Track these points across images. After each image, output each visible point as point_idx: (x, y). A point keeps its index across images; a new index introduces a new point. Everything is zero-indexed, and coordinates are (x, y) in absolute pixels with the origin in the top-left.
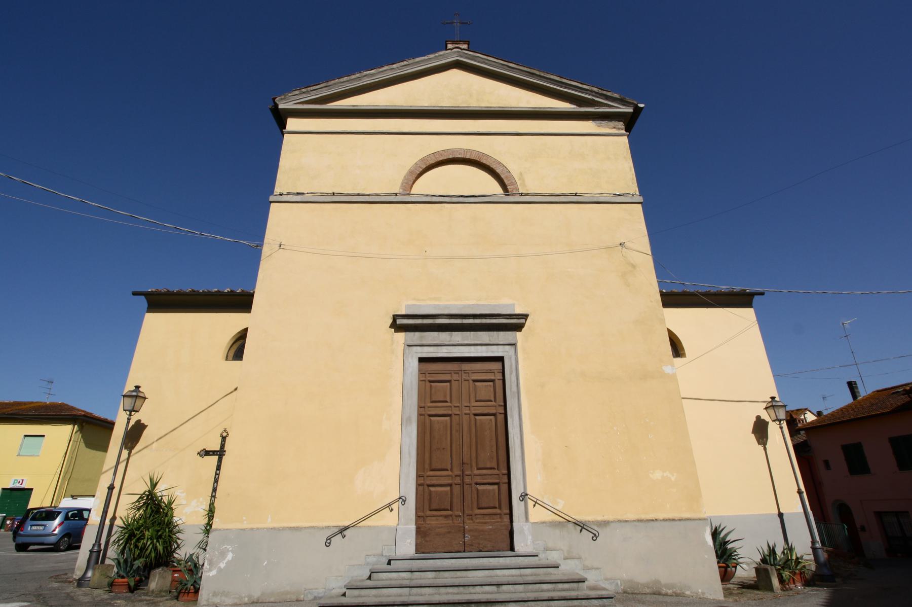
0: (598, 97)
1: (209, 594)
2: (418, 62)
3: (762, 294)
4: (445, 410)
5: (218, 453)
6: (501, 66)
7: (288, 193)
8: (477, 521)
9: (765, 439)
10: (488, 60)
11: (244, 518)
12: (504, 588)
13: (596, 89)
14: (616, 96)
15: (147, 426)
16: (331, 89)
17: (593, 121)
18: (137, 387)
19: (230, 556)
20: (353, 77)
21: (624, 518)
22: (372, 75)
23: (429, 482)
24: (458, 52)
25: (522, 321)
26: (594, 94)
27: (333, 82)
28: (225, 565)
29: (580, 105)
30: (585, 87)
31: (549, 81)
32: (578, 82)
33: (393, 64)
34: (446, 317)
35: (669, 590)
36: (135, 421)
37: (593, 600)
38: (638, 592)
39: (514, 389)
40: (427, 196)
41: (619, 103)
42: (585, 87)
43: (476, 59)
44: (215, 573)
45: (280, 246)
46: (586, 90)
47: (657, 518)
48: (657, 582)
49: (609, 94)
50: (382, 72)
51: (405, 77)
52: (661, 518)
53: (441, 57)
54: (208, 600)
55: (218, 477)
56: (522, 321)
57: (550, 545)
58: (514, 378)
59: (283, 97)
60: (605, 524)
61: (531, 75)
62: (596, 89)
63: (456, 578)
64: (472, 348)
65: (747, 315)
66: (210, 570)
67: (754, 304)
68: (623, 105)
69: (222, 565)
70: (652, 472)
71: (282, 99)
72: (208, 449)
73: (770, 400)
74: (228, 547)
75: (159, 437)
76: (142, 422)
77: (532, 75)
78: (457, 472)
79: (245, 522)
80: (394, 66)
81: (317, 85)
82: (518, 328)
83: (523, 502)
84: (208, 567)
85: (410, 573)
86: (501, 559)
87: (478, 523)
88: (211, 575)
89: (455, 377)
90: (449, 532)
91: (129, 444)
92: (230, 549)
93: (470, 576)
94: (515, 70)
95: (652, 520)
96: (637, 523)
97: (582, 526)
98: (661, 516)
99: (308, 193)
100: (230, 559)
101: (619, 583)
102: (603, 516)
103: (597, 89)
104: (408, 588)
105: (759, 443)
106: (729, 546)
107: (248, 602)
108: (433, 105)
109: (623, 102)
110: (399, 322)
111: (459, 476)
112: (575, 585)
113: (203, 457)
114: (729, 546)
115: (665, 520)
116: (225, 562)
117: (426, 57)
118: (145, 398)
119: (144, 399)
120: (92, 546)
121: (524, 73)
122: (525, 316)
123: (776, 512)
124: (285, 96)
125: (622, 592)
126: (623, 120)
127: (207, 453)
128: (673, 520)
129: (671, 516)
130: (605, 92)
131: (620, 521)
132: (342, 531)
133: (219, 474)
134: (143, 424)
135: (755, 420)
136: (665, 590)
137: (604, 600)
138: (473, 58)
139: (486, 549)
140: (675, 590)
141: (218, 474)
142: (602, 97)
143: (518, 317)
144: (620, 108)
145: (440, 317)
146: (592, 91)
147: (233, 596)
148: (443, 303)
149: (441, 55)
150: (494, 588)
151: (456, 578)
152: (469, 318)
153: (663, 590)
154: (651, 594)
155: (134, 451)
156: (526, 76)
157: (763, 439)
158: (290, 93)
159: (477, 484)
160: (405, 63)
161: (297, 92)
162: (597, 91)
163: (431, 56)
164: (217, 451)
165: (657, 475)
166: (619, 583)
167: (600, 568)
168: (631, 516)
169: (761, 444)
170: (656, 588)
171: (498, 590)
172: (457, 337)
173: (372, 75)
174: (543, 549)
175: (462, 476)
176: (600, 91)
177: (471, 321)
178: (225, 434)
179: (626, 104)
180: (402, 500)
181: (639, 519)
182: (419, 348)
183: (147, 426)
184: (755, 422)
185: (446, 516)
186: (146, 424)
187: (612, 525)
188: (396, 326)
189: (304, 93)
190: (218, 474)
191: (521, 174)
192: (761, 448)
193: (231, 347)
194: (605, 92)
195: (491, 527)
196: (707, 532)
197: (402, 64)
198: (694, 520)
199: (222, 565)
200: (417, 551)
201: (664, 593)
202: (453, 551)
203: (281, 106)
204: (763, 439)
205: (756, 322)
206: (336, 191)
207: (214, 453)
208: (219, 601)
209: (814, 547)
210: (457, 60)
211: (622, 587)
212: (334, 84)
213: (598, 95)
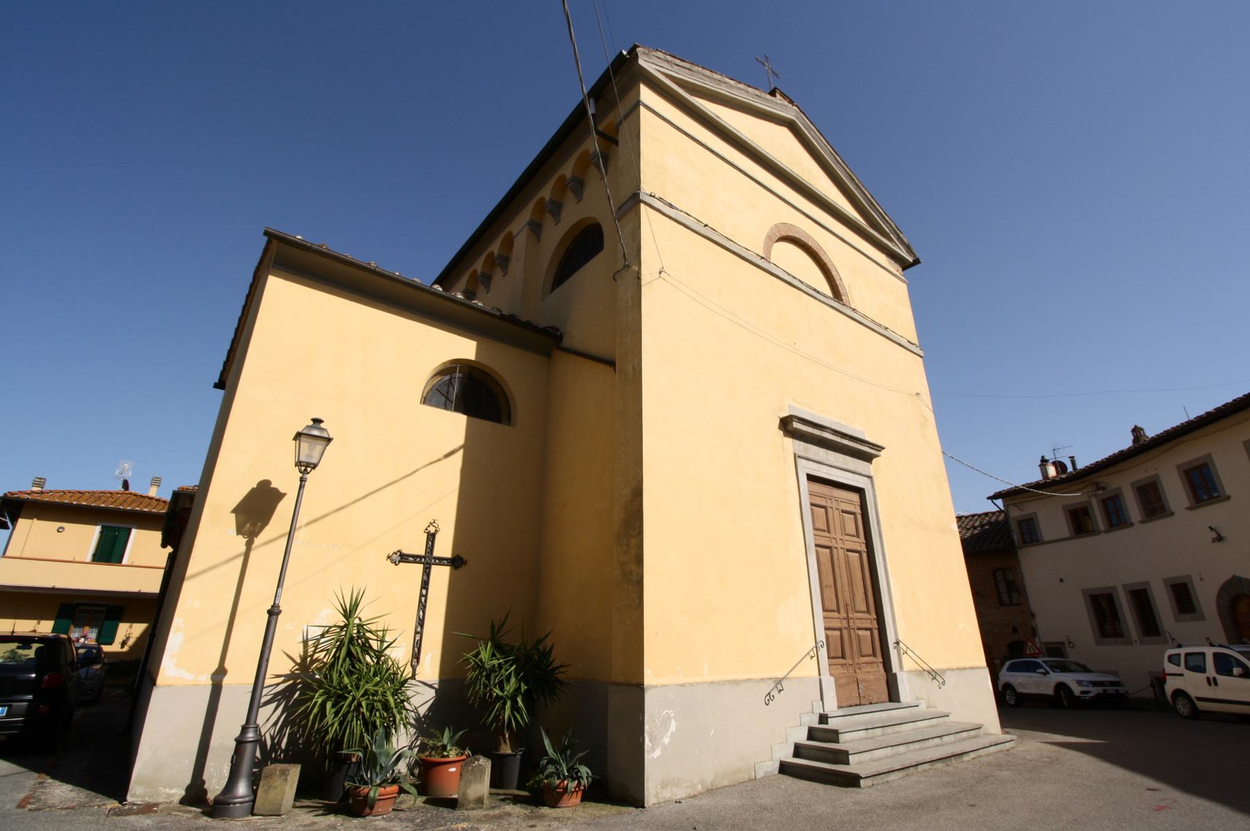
1: (657, 787)
4: (826, 541)
5: (423, 560)
6: (829, 152)
7: (660, 199)
10: (820, 139)
11: (679, 669)
12: (945, 739)
15: (285, 494)
16: (692, 76)
18: (317, 421)
19: (673, 726)
20: (715, 76)
21: (962, 665)
24: (797, 112)
25: (874, 452)
26: (891, 229)
28: (669, 739)
34: (830, 431)
40: (789, 274)
43: (810, 130)
44: (660, 753)
45: (660, 273)
46: (887, 222)
51: (772, 116)
54: (656, 796)
55: (426, 601)
56: (874, 452)
66: (653, 750)
68: (908, 252)
69: (666, 740)
72: (405, 551)
73: (311, 423)
74: (670, 712)
75: (313, 518)
76: (272, 486)
78: (843, 615)
79: (681, 675)
84: (650, 745)
85: (864, 731)
88: (655, 757)
90: (848, 683)
91: (248, 525)
92: (672, 715)
99: (681, 211)
100: (674, 730)
104: (890, 748)
107: (702, 791)
108: (774, 156)
110: (796, 425)
112: (972, 733)
113: (396, 565)
116: (669, 734)
118: (329, 440)
119: (324, 443)
120: (240, 728)
122: (880, 448)
124: (649, 52)
127: (404, 558)
133: (426, 596)
134: (276, 490)
141: (423, 596)
144: (901, 250)
147: (685, 784)
150: (938, 739)
155: (258, 541)
164: (432, 553)
173: (731, 86)
175: (848, 619)
177: (846, 442)
178: (432, 530)
183: (285, 494)
186: (282, 491)
188: (786, 425)
189: (667, 61)
190: (423, 596)
191: (849, 286)
193: (429, 381)
199: (666, 740)
207: (415, 559)
208: (670, 795)
210: (794, 121)
212: (698, 72)
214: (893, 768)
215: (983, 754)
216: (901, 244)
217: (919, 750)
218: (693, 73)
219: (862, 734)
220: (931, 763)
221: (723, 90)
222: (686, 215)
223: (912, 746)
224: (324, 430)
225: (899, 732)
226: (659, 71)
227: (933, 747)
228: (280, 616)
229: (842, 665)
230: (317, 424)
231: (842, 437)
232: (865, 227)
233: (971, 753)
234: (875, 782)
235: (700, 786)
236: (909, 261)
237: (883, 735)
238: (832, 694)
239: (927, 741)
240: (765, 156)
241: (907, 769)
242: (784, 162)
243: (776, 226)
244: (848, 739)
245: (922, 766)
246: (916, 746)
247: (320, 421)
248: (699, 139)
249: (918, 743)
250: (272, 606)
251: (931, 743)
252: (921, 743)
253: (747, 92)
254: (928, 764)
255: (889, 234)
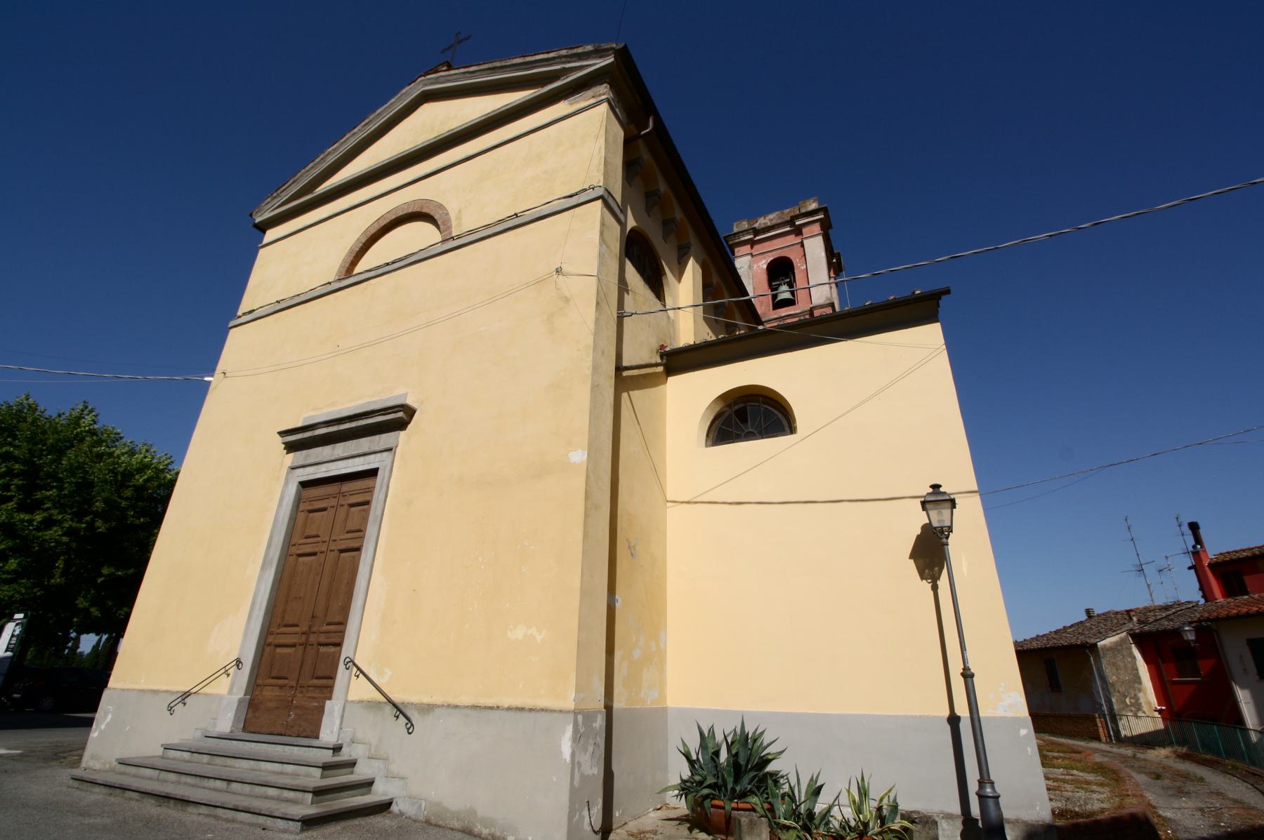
0: (569, 62)
2: (379, 114)
3: (947, 292)
4: (313, 547)
6: (463, 76)
8: (308, 695)
9: (936, 569)
10: (450, 75)
12: (234, 786)
13: (564, 52)
14: (589, 48)
17: (565, 100)
20: (317, 160)
22: (335, 150)
23: (276, 642)
26: (563, 60)
27: (299, 174)
29: (543, 85)
30: (552, 55)
31: (512, 68)
32: (543, 53)
33: (354, 128)
34: (324, 425)
35: (486, 829)
36: (939, 586)
37: (279, 820)
38: (444, 825)
39: (379, 513)
41: (595, 58)
42: (552, 55)
46: (553, 58)
47: (500, 704)
48: (472, 812)
49: (580, 50)
50: (345, 141)
52: (506, 706)
53: (404, 96)
57: (359, 735)
58: (382, 496)
59: (257, 210)
60: (428, 708)
61: (493, 71)
62: (564, 52)
63: (225, 766)
64: (350, 461)
65: (930, 336)
67: (940, 315)
68: (601, 57)
69: (103, 727)
70: (512, 627)
71: (257, 212)
73: (931, 490)
77: (493, 69)
79: (128, 682)
80: (356, 130)
81: (286, 184)
82: (401, 425)
83: (348, 671)
86: (296, 748)
87: (309, 697)
89: (333, 502)
90: (277, 708)
93: (237, 765)
94: (477, 74)
95: (491, 708)
96: (468, 711)
97: (399, 710)
98: (506, 702)
101: (423, 804)
102: (432, 697)
103: (565, 51)
105: (922, 578)
106: (770, 768)
108: (375, 163)
109: (598, 53)
111: (305, 634)
114: (770, 768)
115: (509, 709)
116: (105, 723)
117: (388, 104)
121: (485, 72)
123: (947, 713)
125: (424, 821)
126: (608, 80)
128: (522, 709)
129: (519, 702)
130: (575, 51)
131: (449, 706)
132: (186, 695)
135: (919, 532)
136: (479, 827)
137: (290, 822)
138: (436, 81)
139: (305, 734)
140: (493, 830)
142: (574, 59)
143: (393, 410)
145: (318, 426)
146: (560, 57)
148: (339, 408)
149: (403, 94)
150: (225, 784)
151: (225, 766)
152: (346, 423)
153: (477, 827)
154: (459, 831)
156: (471, 78)
157: (932, 569)
158: (263, 203)
159: (320, 644)
160: (367, 121)
161: (269, 199)
162: (565, 54)
163: (393, 100)
165: (518, 633)
166: (423, 804)
167: (407, 778)
168: (466, 700)
169: (926, 579)
170: (468, 822)
171: (227, 788)
172: (340, 449)
173: (335, 150)
174: (349, 740)
176: (571, 52)
179: (603, 53)
180: (238, 662)
181: (476, 705)
182: (301, 470)
184: (918, 537)
185: (281, 687)
187: (438, 711)
192: (926, 586)
194: (575, 51)
195: (316, 704)
196: (566, 734)
197: (363, 123)
198: (552, 711)
199: (103, 727)
200: (245, 729)
201: (476, 833)
202: (275, 733)
203: (258, 220)
204: (932, 569)
205: (944, 347)
206: (278, 299)
209: (982, 793)
210: (423, 92)
211: (426, 813)
212: (301, 176)
213: (569, 59)
214: (95, 780)
215: (223, 816)
216: (587, 59)
217: (193, 786)
218: (299, 181)
219: (186, 755)
220: (143, 795)
221: (331, 159)
222: (261, 309)
223: (184, 779)
224: (944, 493)
225: (230, 767)
226: (273, 210)
227: (210, 789)
228: (975, 679)
229: (281, 687)
230: (936, 490)
231: (350, 422)
232: (538, 93)
233: (203, 807)
234: (80, 787)
235: (108, 765)
236: (613, 62)
237: (209, 764)
238: (230, 715)
239: (206, 780)
240: (355, 179)
241: (212, 808)
242: (407, 148)
243: (441, 206)
244: (171, 757)
245: (130, 792)
246: (189, 780)
247: (939, 486)
248: (345, 214)
249: (194, 777)
250: (964, 669)
251: (212, 783)
252: (198, 779)
253: (354, 134)
254: (137, 794)
255: (564, 68)
